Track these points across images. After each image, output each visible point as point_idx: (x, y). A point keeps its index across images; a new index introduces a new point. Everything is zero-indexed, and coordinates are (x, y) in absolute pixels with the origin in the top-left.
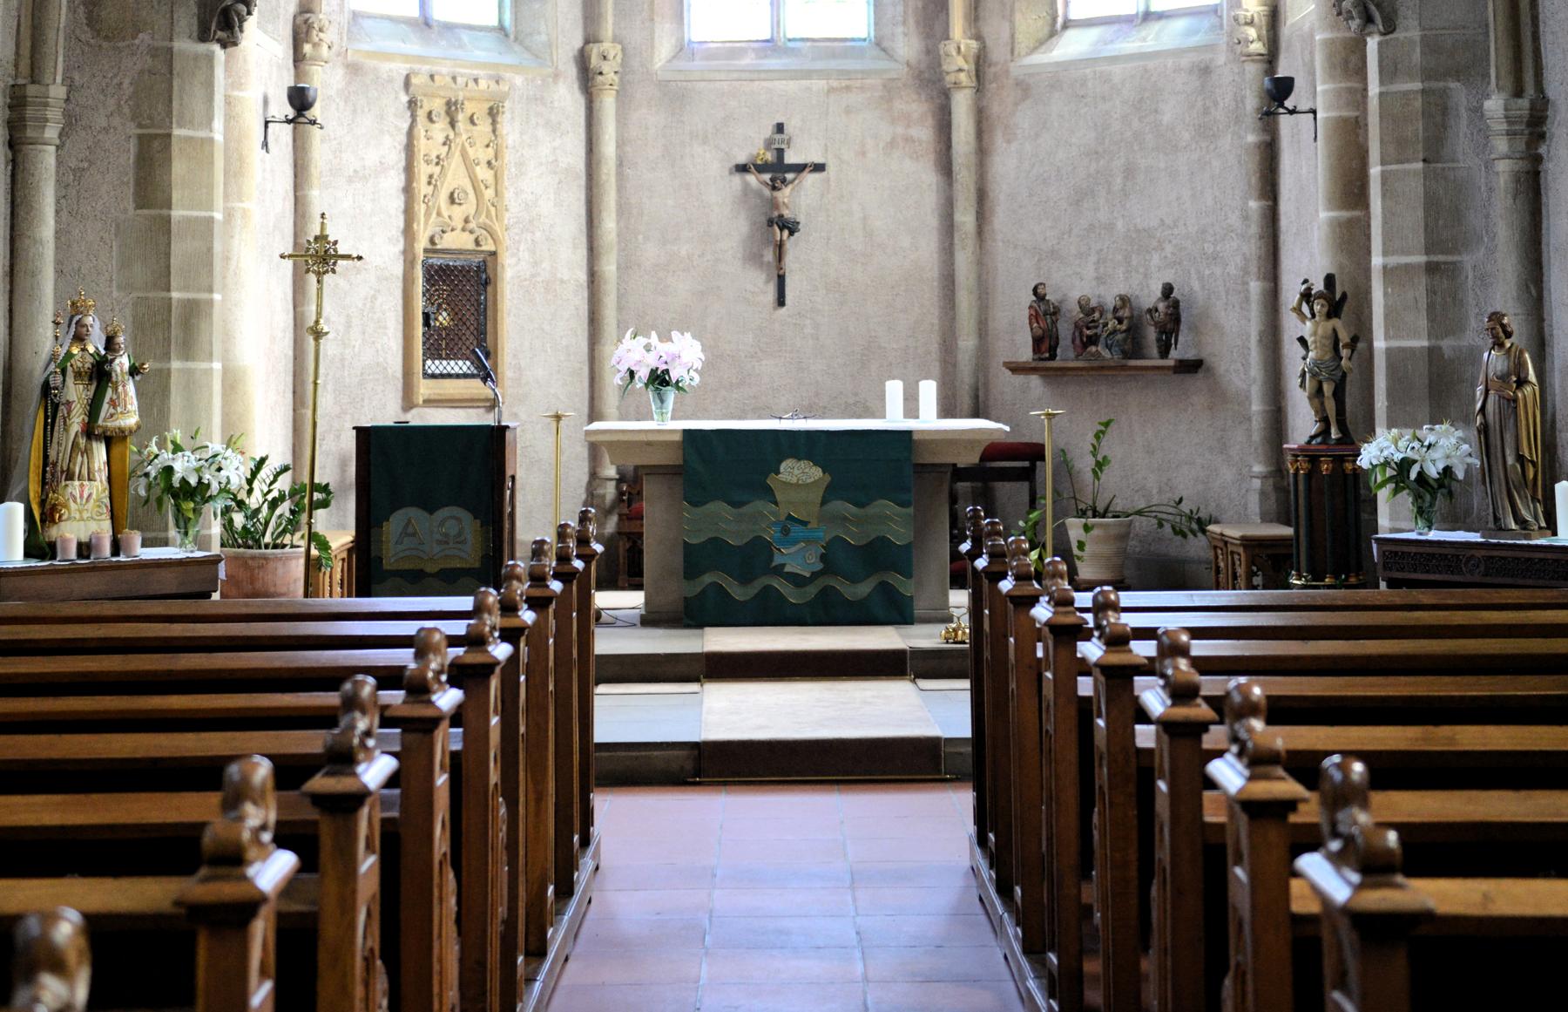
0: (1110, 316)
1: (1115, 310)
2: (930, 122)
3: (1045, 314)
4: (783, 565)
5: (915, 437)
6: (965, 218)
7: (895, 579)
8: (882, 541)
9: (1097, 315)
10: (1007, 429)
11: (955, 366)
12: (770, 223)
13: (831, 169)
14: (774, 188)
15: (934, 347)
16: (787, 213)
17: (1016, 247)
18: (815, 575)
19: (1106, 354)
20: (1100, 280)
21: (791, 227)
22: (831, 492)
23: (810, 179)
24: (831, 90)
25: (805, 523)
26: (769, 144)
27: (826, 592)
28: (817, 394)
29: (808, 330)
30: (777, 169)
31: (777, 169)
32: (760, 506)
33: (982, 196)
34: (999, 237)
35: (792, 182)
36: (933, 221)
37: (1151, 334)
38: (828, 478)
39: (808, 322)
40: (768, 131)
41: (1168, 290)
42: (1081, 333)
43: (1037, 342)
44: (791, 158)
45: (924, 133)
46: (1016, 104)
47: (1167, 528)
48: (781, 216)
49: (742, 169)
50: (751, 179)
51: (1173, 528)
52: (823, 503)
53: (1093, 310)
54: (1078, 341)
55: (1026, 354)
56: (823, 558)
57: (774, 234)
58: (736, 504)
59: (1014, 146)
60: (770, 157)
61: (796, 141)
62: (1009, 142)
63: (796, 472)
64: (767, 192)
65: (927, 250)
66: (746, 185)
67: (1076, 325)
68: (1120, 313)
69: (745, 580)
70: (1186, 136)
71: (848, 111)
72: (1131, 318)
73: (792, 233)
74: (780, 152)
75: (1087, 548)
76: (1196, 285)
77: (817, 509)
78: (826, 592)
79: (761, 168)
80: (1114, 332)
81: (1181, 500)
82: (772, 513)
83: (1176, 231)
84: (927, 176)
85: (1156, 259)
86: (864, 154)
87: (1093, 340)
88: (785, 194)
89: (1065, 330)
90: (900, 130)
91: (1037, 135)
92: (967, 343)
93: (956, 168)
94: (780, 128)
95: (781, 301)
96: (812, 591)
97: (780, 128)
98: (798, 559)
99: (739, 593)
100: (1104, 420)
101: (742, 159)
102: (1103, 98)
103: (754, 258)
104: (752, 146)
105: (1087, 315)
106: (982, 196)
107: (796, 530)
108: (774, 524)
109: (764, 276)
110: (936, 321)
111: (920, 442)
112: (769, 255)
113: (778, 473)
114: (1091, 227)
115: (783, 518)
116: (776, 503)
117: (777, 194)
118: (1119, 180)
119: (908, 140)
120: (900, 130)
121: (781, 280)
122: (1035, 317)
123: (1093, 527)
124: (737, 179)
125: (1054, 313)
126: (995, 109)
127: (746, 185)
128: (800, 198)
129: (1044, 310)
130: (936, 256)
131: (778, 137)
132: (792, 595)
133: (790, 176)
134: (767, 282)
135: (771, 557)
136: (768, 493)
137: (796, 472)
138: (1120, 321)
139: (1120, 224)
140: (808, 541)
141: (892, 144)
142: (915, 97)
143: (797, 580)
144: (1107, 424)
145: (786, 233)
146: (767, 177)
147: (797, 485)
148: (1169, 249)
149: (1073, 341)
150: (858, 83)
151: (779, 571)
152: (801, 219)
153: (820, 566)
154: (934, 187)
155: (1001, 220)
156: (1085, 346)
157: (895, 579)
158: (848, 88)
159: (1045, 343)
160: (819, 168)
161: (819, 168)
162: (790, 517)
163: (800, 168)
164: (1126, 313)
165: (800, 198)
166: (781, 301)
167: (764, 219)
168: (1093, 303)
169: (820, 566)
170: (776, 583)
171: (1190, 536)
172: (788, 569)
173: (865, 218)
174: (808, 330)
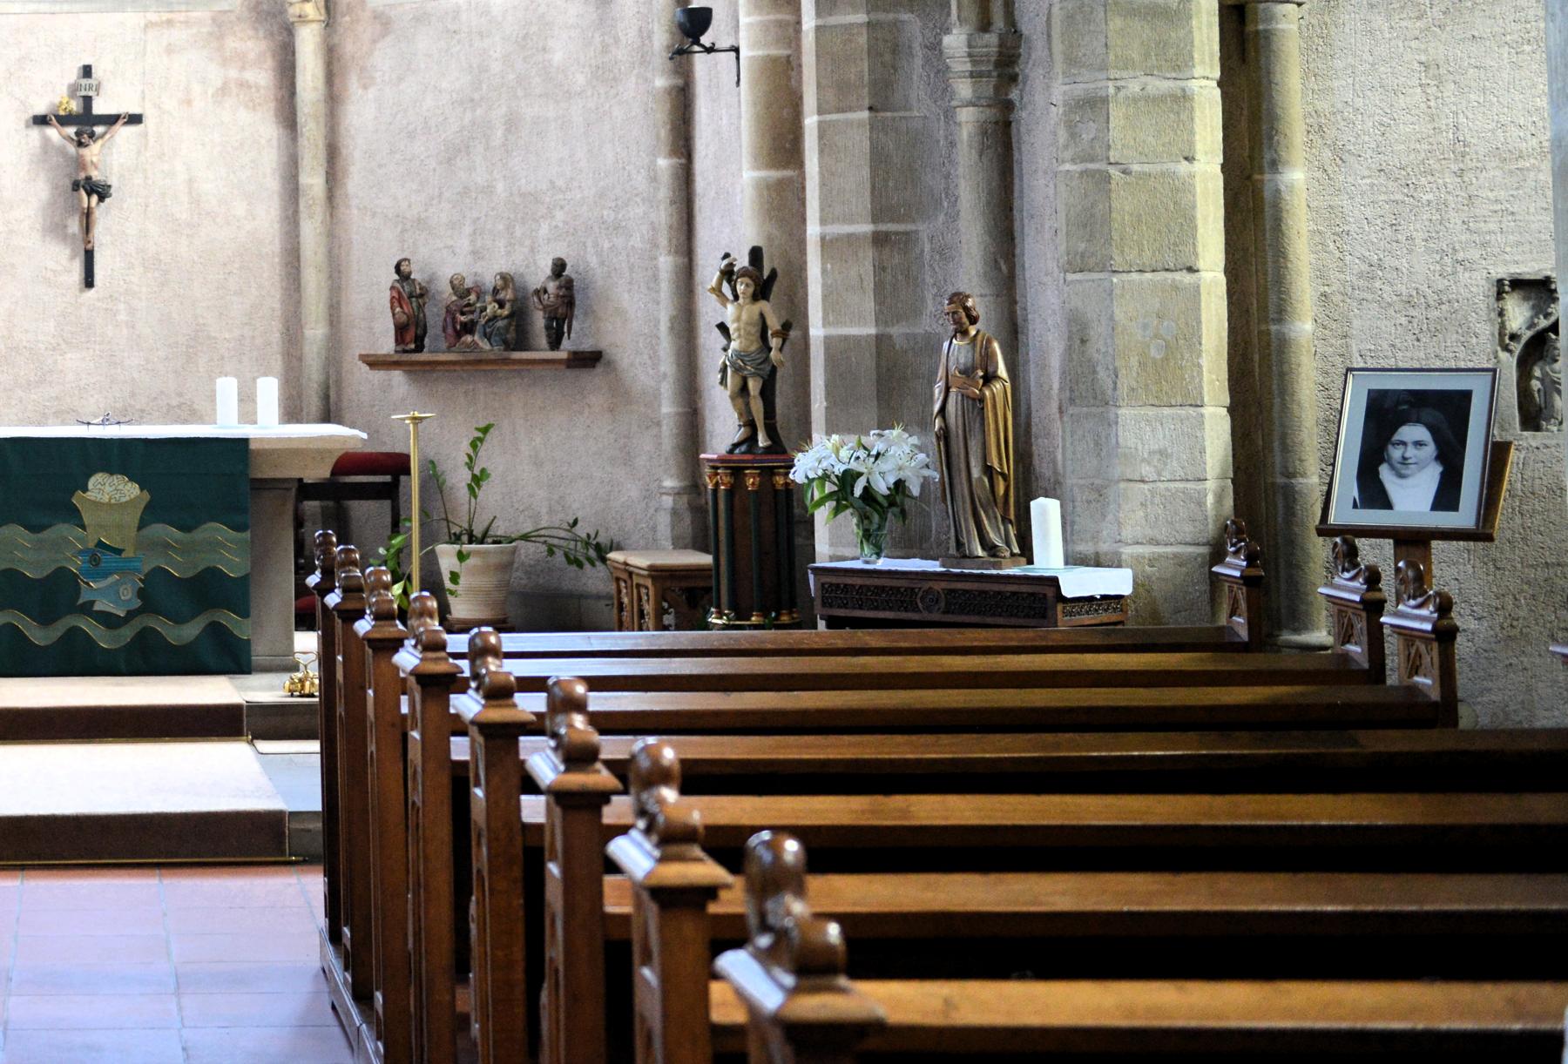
0: (489, 298)
1: (496, 291)
2: (269, 63)
3: (411, 296)
4: (92, 603)
5: (252, 446)
6: (313, 180)
7: (228, 619)
8: (212, 574)
9: (473, 297)
10: (365, 436)
11: (300, 359)
12: (76, 186)
13: (149, 121)
14: (80, 144)
15: (276, 337)
16: (96, 175)
17: (374, 215)
18: (131, 615)
19: (485, 345)
20: (476, 254)
21: (101, 191)
22: (151, 513)
23: (123, 132)
24: (149, 25)
25: (119, 552)
26: (73, 90)
27: (145, 635)
28: (133, 395)
29: (122, 317)
30: (84, 121)
31: (84, 121)
32: (63, 530)
33: (333, 154)
34: (354, 202)
35: (102, 136)
36: (272, 183)
37: (539, 321)
38: (146, 496)
39: (122, 306)
40: (73, 75)
41: (559, 267)
42: (454, 319)
43: (401, 331)
44: (99, 108)
45: (263, 77)
46: (374, 42)
47: (559, 557)
48: (88, 178)
49: (41, 121)
50: (53, 133)
51: (566, 555)
52: (140, 528)
53: (468, 292)
54: (450, 330)
55: (386, 344)
56: (141, 593)
57: (80, 200)
58: (35, 528)
59: (372, 93)
60: (75, 106)
61: (107, 88)
62: (365, 87)
63: (108, 489)
64: (72, 149)
65: (266, 218)
66: (46, 141)
67: (448, 310)
68: (501, 296)
69: (46, 620)
70: (581, 79)
71: (170, 50)
72: (514, 301)
73: (102, 198)
74: (88, 101)
75: (462, 581)
76: (593, 261)
77: (133, 533)
78: (145, 635)
79: (64, 120)
80: (494, 318)
81: (576, 522)
82: (78, 539)
83: (569, 196)
84: (268, 130)
85: (544, 230)
86: (189, 102)
87: (469, 328)
88: (93, 152)
89: (434, 316)
90: (233, 73)
91: (400, 79)
92: (315, 332)
93: (301, 119)
94: (87, 71)
95: (89, 282)
96: (127, 633)
97: (87, 71)
98: (111, 594)
99: (39, 636)
100: (482, 425)
101: (41, 110)
102: (481, 34)
103: (55, 229)
104: (54, 93)
105: (461, 297)
106: (333, 154)
107: (107, 559)
108: (81, 552)
109: (68, 251)
110: (277, 306)
111: (259, 453)
112: (74, 226)
113: (85, 490)
114: (466, 191)
115: (91, 545)
116: (83, 527)
117: (84, 151)
118: (499, 133)
119: (243, 85)
120: (233, 73)
121: (89, 257)
122: (397, 300)
123: (468, 555)
124: (35, 133)
125: (421, 296)
126: (349, 48)
127: (46, 141)
128: (112, 156)
129: (409, 293)
130: (277, 226)
131: (85, 82)
132: (104, 639)
133: (99, 130)
134: (72, 258)
135: (77, 591)
136: (73, 515)
137: (108, 489)
138: (501, 305)
139: (500, 187)
140: (122, 571)
141: (223, 90)
142: (251, 33)
143: (108, 620)
144: (485, 430)
145: (95, 198)
146: (71, 131)
147: (109, 505)
148: (559, 215)
149: (444, 330)
150: (181, 17)
151: (87, 609)
152: (113, 181)
153: (137, 603)
154: (275, 143)
155: (355, 182)
156: (459, 335)
157: (228, 619)
158: (170, 22)
159: (410, 332)
160: (135, 119)
161: (135, 119)
162: (100, 544)
163: (111, 120)
164: (508, 295)
165: (112, 156)
166: (89, 282)
167: (68, 183)
168: (469, 283)
169: (137, 603)
170: (88, 626)
171: (587, 566)
172: (97, 607)
173: (190, 181)
174: (122, 317)
